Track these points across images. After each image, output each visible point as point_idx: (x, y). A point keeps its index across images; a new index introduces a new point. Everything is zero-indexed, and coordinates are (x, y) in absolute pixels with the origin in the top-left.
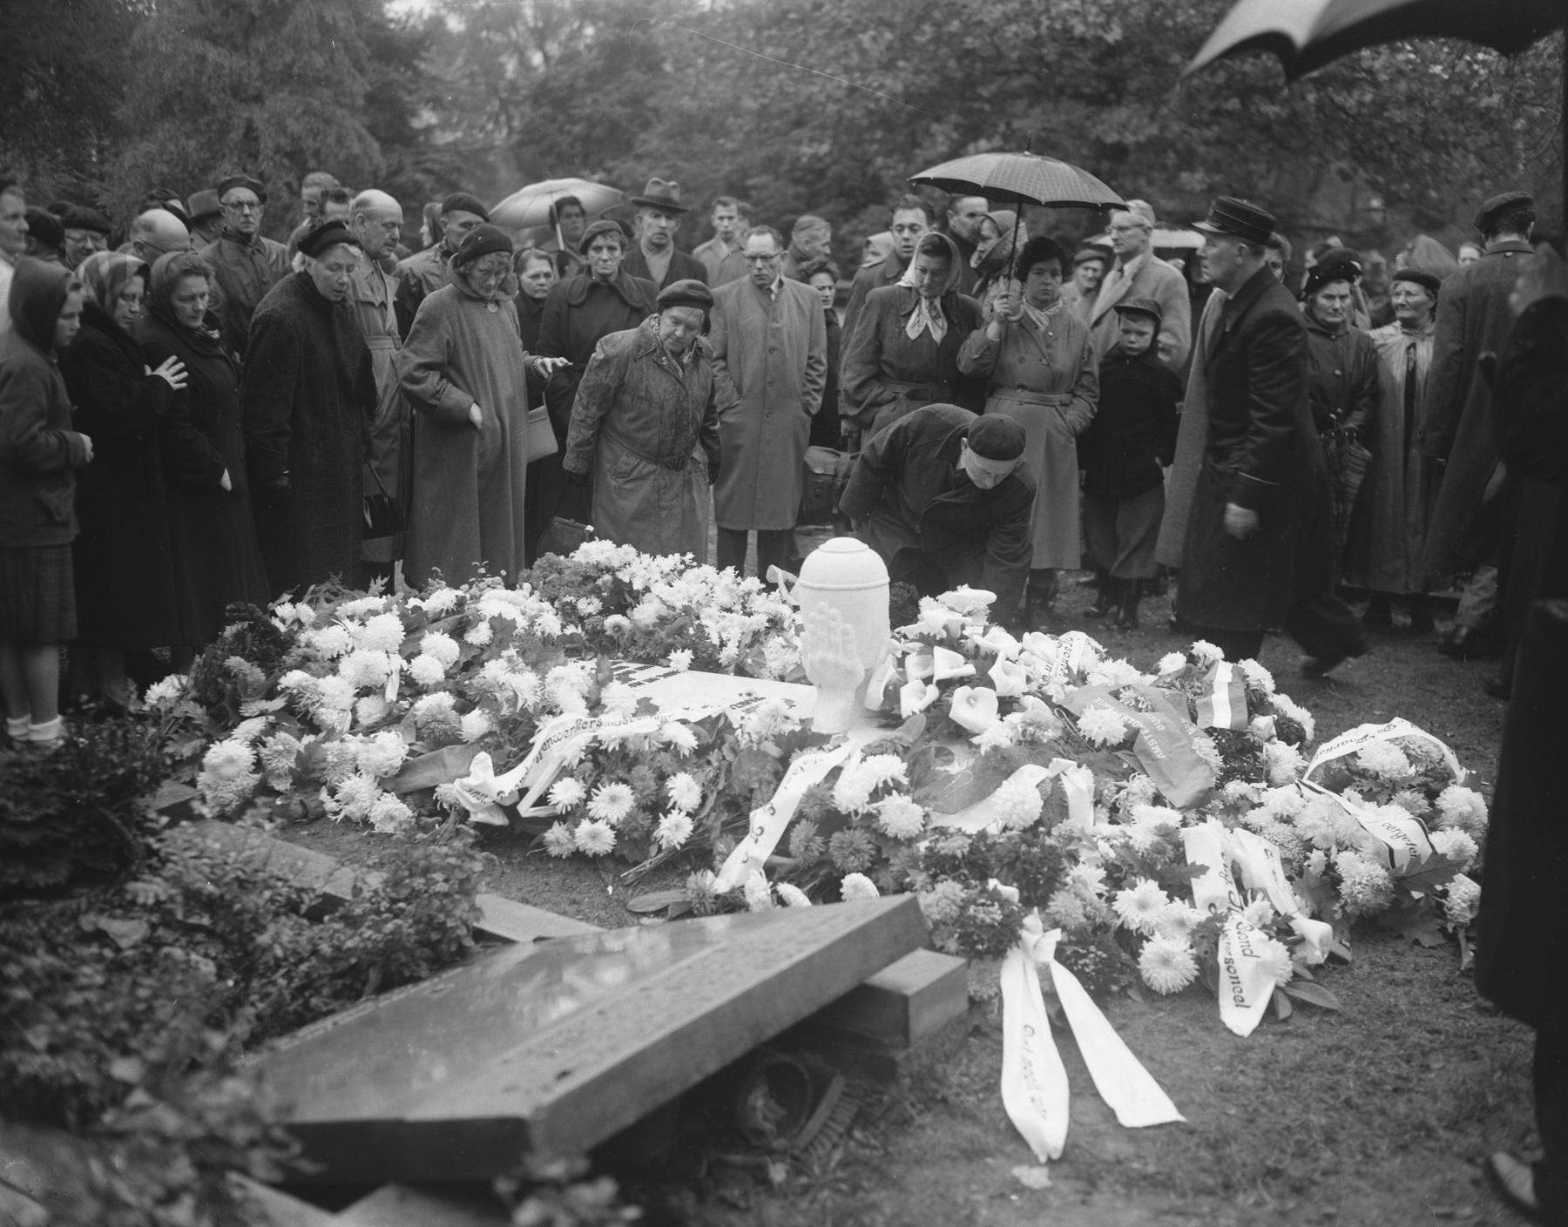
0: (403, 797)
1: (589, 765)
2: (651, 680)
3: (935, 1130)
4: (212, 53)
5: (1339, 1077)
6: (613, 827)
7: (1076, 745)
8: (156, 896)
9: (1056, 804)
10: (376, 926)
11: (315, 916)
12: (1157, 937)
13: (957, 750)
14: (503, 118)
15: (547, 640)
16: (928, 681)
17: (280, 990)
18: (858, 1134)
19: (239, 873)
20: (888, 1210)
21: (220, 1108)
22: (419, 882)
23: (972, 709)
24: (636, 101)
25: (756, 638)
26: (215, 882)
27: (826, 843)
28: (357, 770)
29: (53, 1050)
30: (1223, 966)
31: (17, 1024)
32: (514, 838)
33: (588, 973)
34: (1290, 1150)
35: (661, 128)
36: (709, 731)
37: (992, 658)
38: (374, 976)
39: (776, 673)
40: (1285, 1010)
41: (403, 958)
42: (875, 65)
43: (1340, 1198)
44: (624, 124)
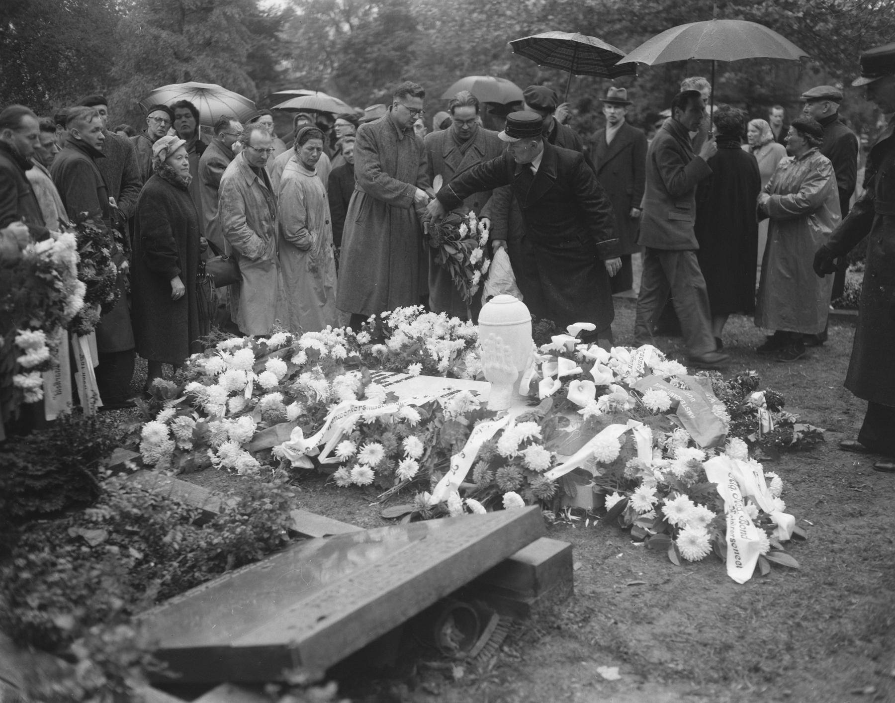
0: (254, 454)
1: (358, 433)
2: (397, 382)
3: (552, 646)
4: (164, 34)
5: (797, 609)
6: (372, 469)
7: (641, 412)
8: (104, 517)
9: (629, 447)
10: (232, 531)
11: (199, 524)
12: (688, 528)
13: (571, 418)
14: (328, 62)
15: (339, 361)
16: (555, 377)
17: (175, 569)
18: (506, 649)
19: (153, 502)
20: (522, 694)
21: (113, 643)
22: (256, 504)
23: (581, 394)
24: (402, 48)
25: (460, 353)
26: (139, 508)
27: (494, 475)
28: (229, 439)
29: (42, 607)
30: (729, 543)
31: (23, 592)
32: (316, 477)
33: (362, 554)
34: (765, 655)
35: (417, 63)
36: (428, 411)
37: (592, 362)
38: (230, 559)
39: (471, 374)
40: (765, 569)
41: (248, 549)
42: (536, 19)
43: (794, 684)
44: (396, 61)
